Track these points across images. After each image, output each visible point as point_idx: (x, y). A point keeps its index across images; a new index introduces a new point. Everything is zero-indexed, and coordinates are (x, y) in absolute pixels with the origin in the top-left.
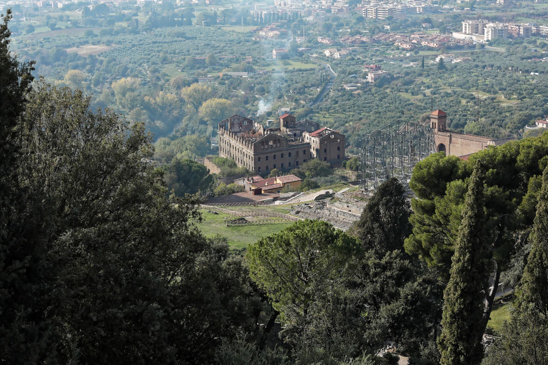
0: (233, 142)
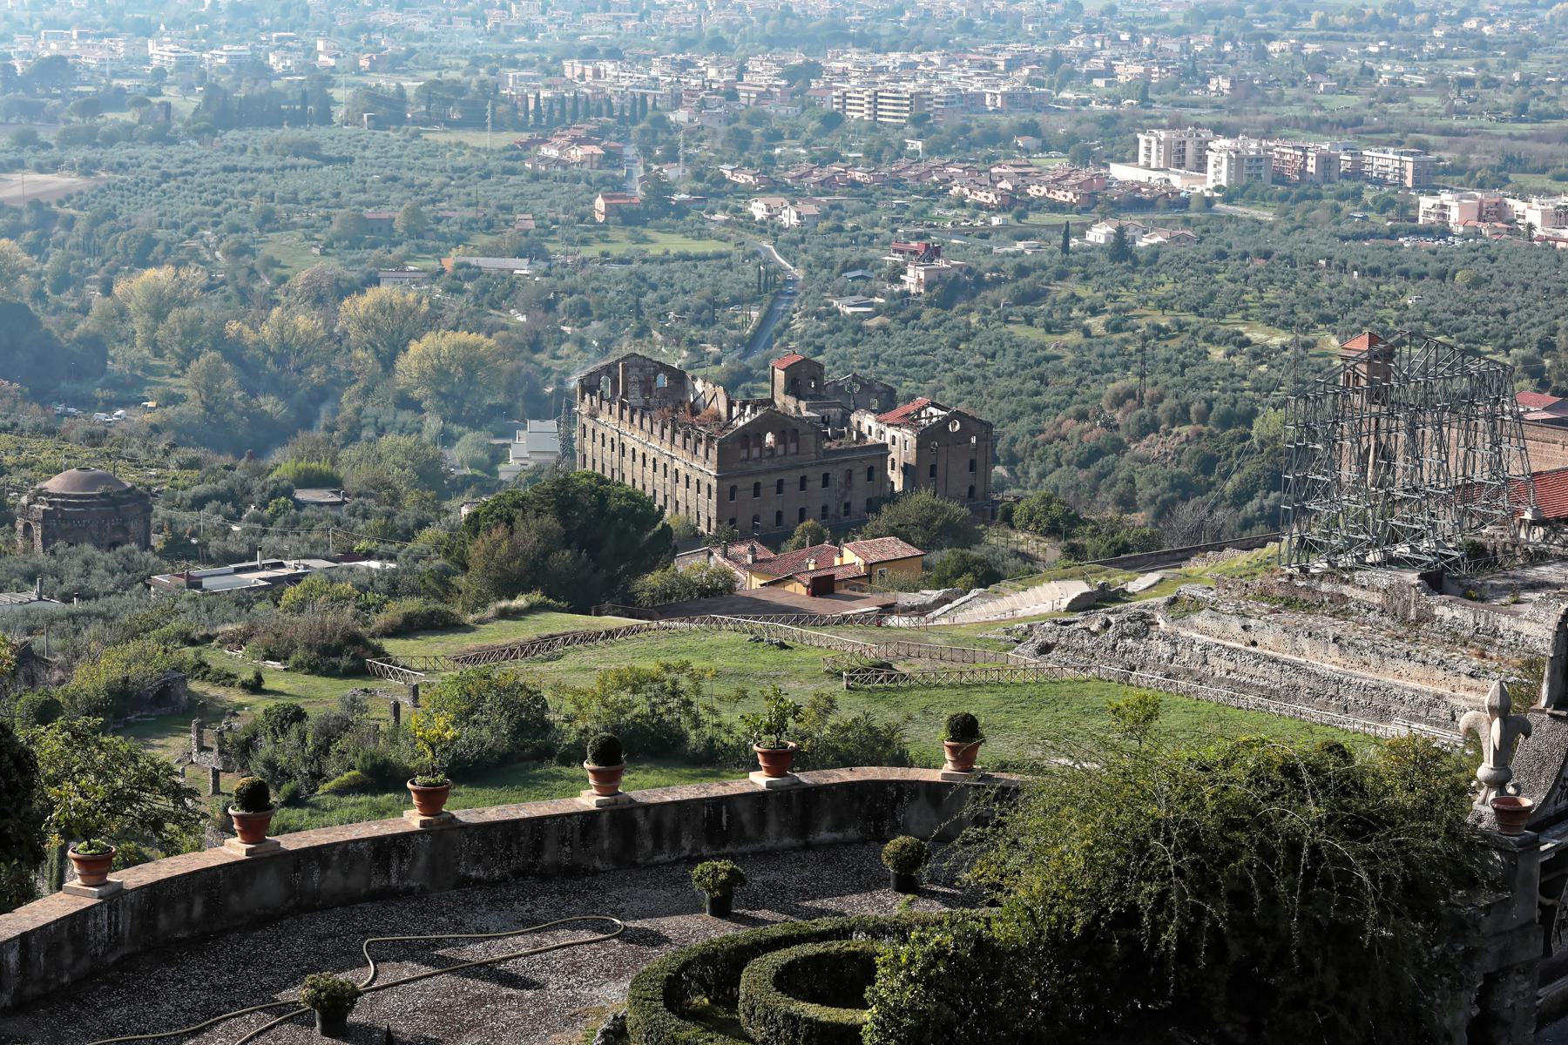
0: (634, 438)
